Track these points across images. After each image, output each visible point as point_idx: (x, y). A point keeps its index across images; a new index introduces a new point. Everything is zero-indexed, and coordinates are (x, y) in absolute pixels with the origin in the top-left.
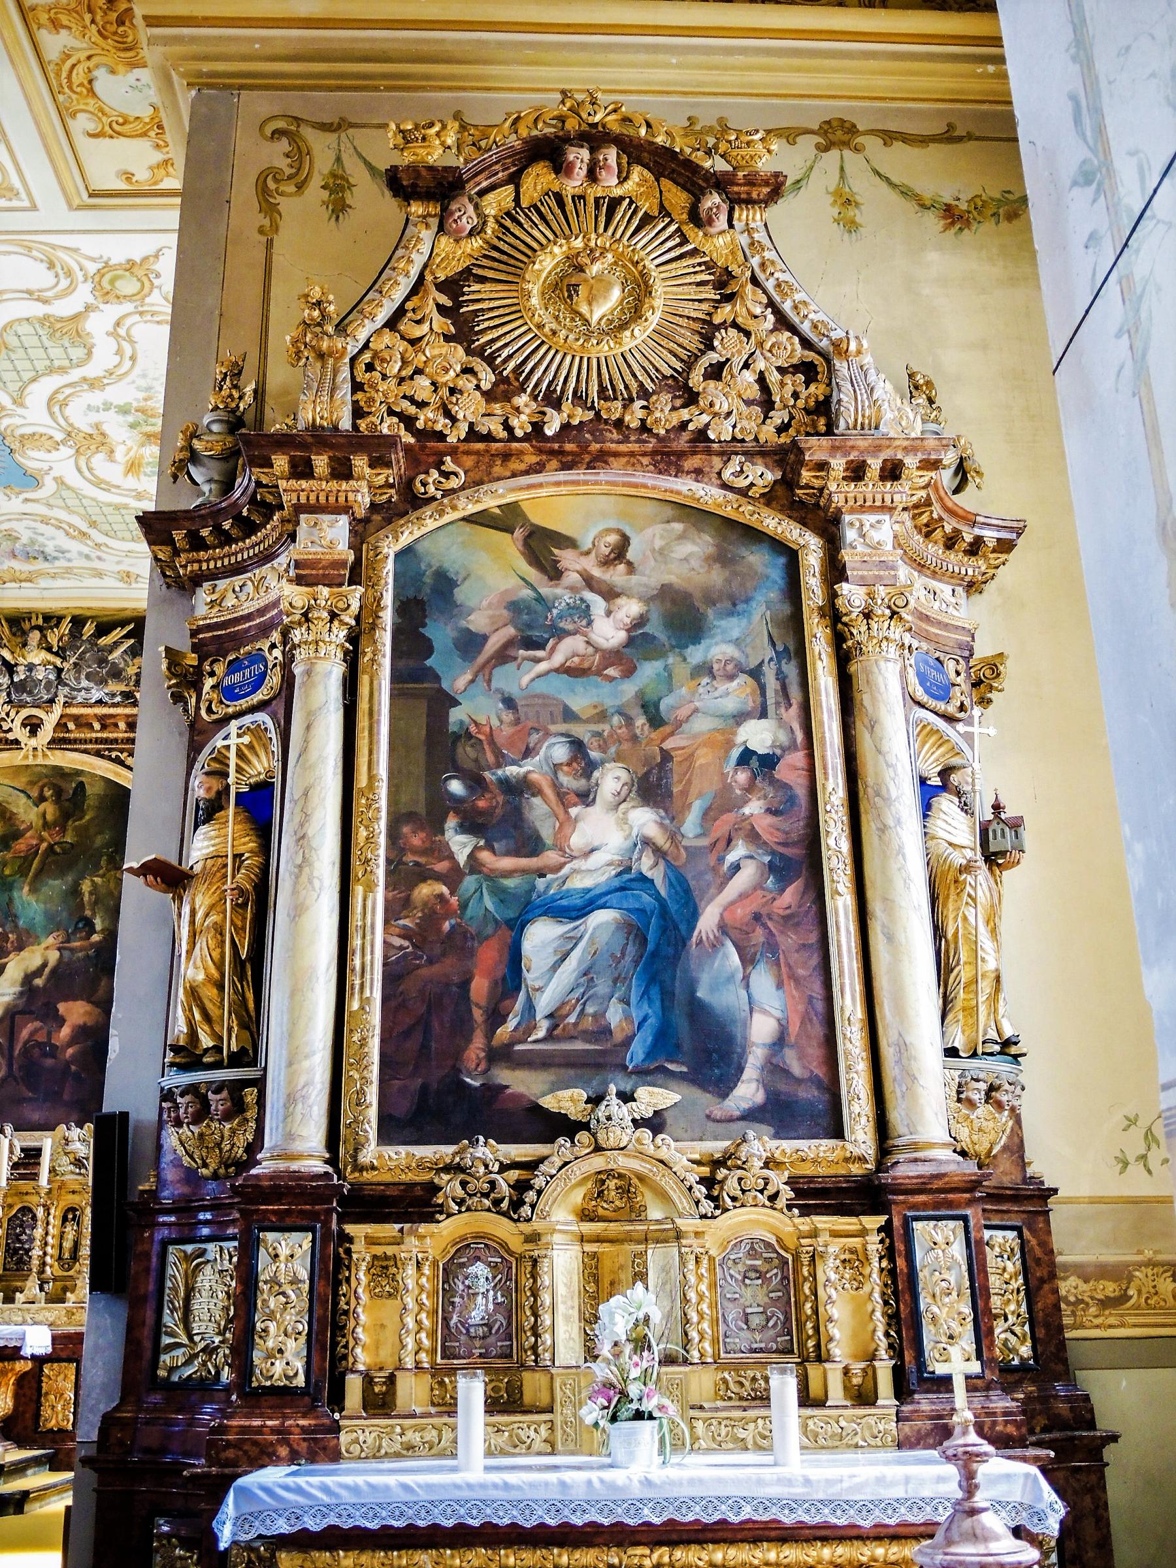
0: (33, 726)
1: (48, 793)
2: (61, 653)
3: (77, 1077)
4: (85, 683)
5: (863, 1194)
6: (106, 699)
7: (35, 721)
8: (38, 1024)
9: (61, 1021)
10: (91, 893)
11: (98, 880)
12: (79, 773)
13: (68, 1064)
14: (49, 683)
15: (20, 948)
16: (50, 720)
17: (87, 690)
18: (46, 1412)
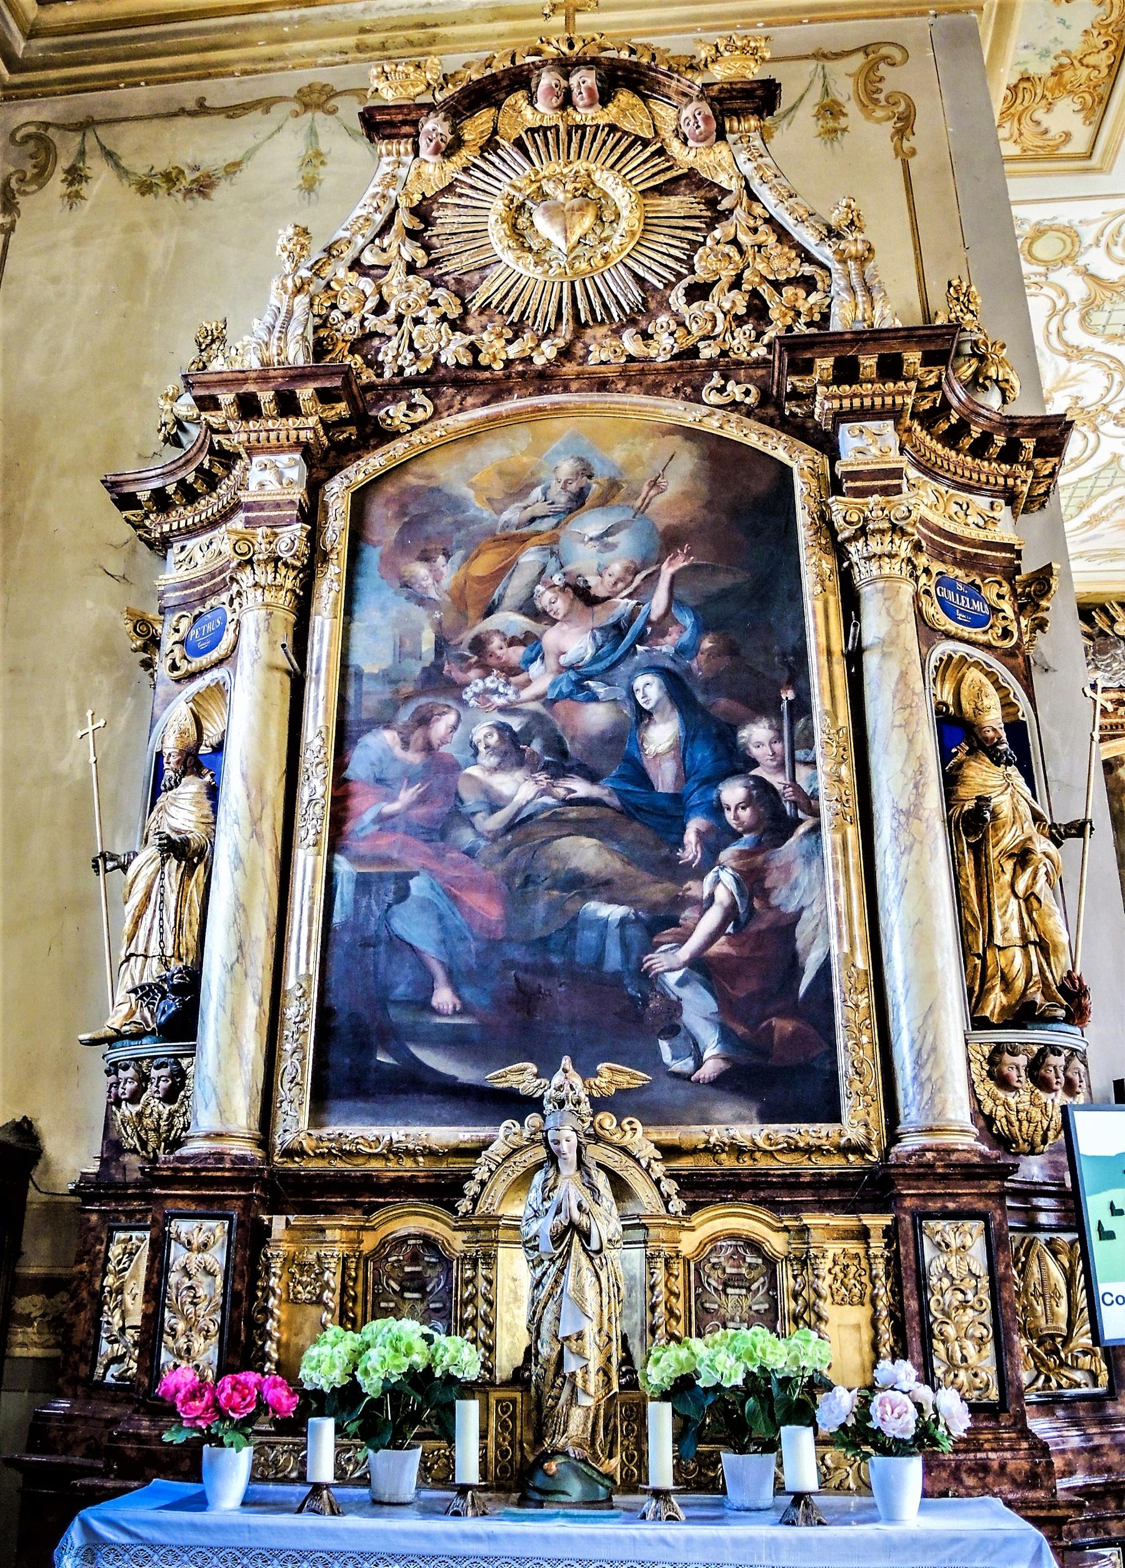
5: (867, 1187)
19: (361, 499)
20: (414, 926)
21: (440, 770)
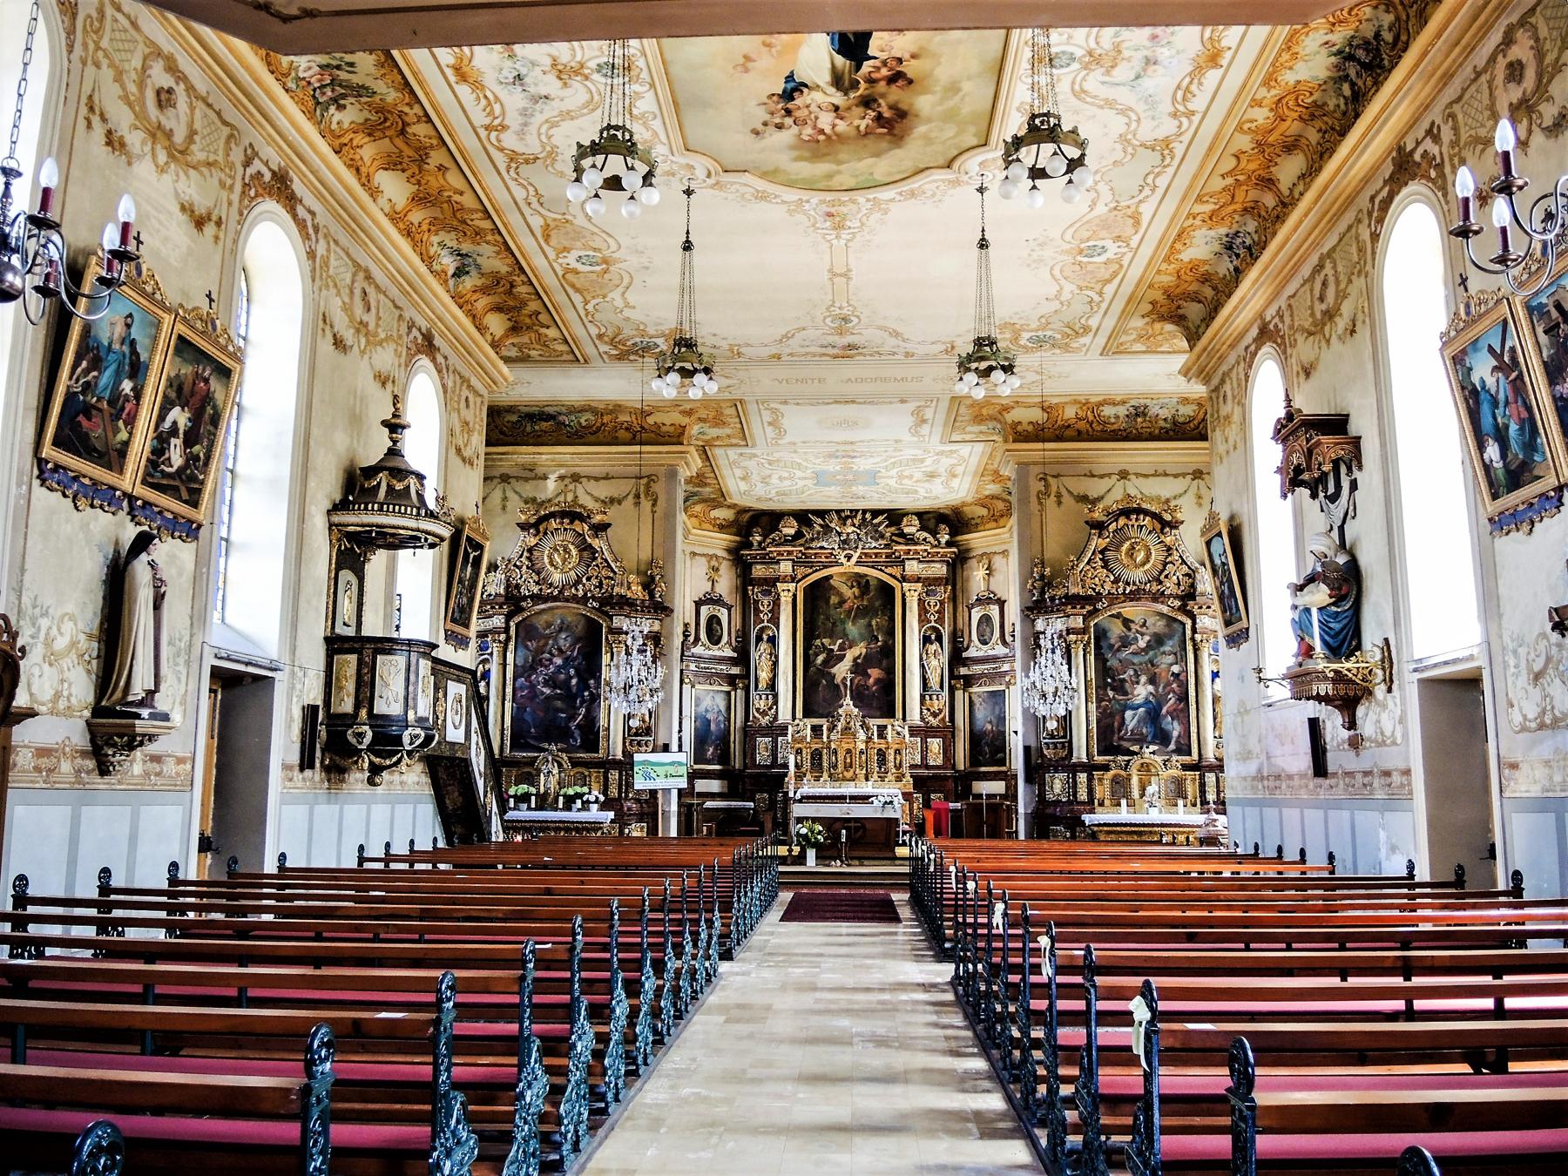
19: (517, 625)
20: (528, 717)
21: (532, 687)
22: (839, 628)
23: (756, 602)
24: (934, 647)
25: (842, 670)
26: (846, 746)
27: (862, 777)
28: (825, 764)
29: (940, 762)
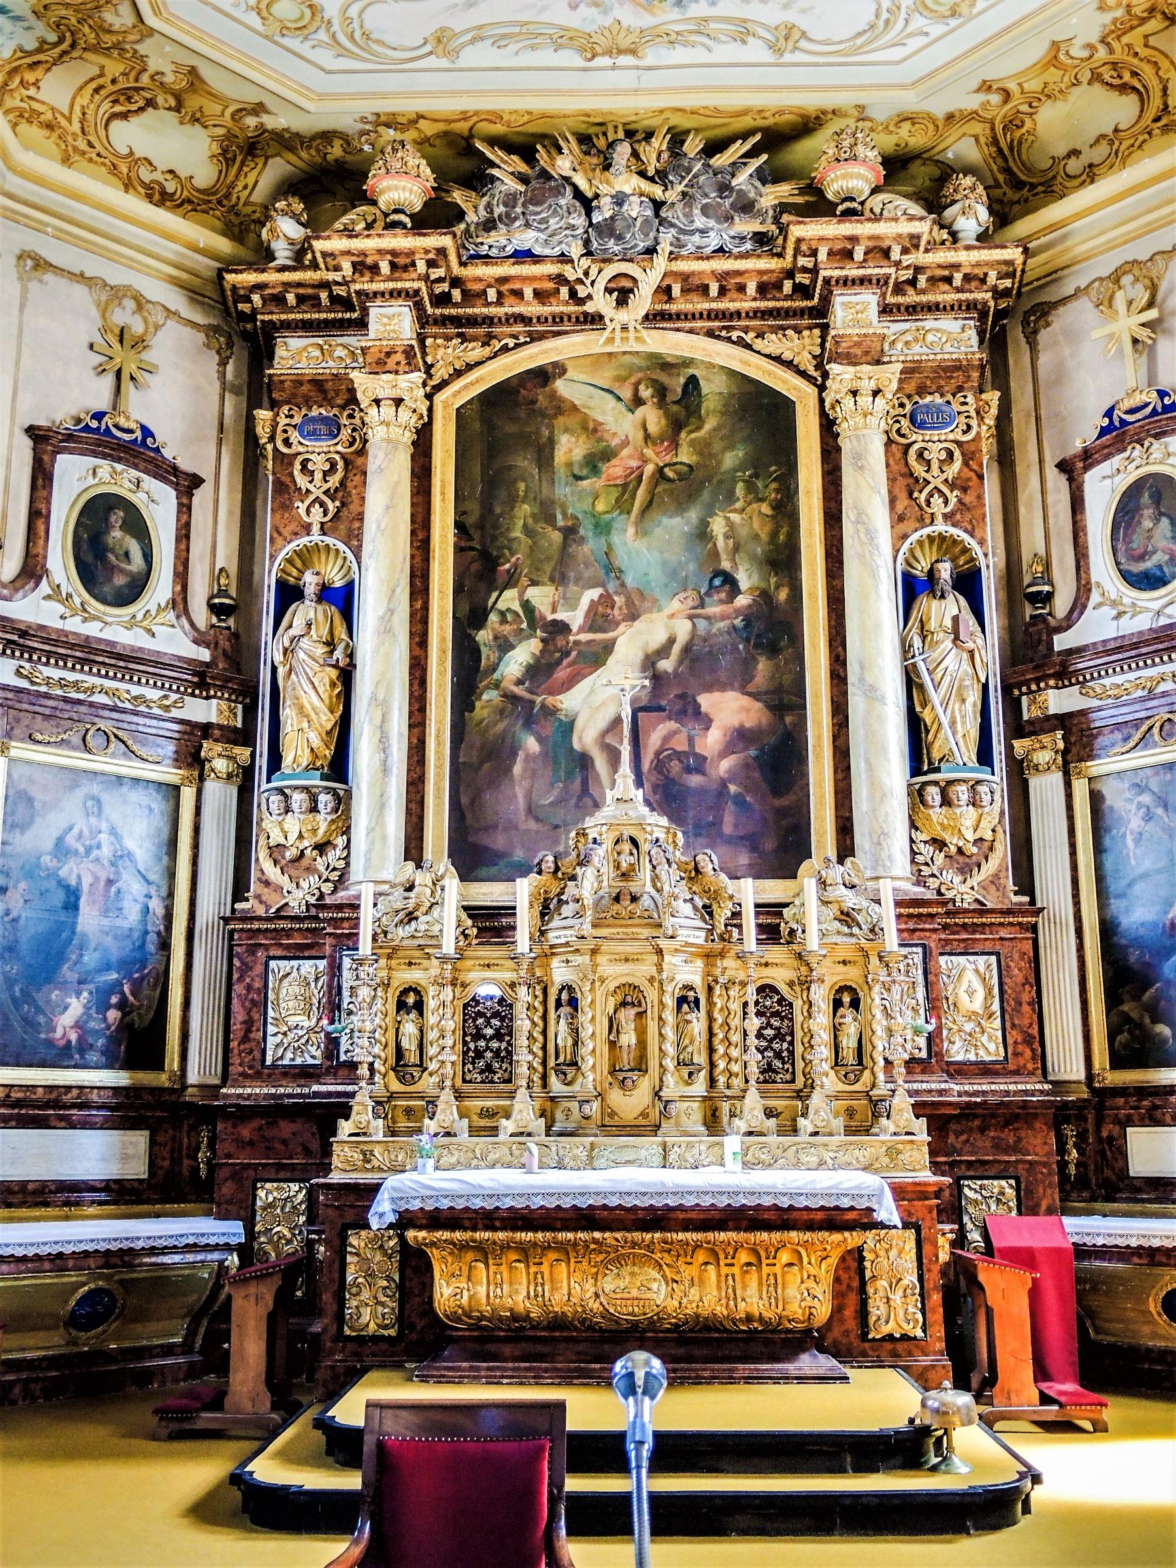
0: (623, 295)
1: (646, 393)
2: (661, 178)
3: (739, 801)
4: (700, 222)
6: (729, 246)
7: (627, 284)
8: (672, 725)
9: (706, 722)
10: (726, 537)
11: (735, 517)
12: (687, 363)
13: (723, 784)
14: (646, 221)
15: (633, 617)
16: (648, 280)
17: (703, 232)
18: (877, 1308)
22: (591, 546)
23: (283, 461)
24: (945, 609)
25: (597, 701)
26: (614, 972)
27: (691, 1115)
28: (524, 1058)
29: (991, 1049)
